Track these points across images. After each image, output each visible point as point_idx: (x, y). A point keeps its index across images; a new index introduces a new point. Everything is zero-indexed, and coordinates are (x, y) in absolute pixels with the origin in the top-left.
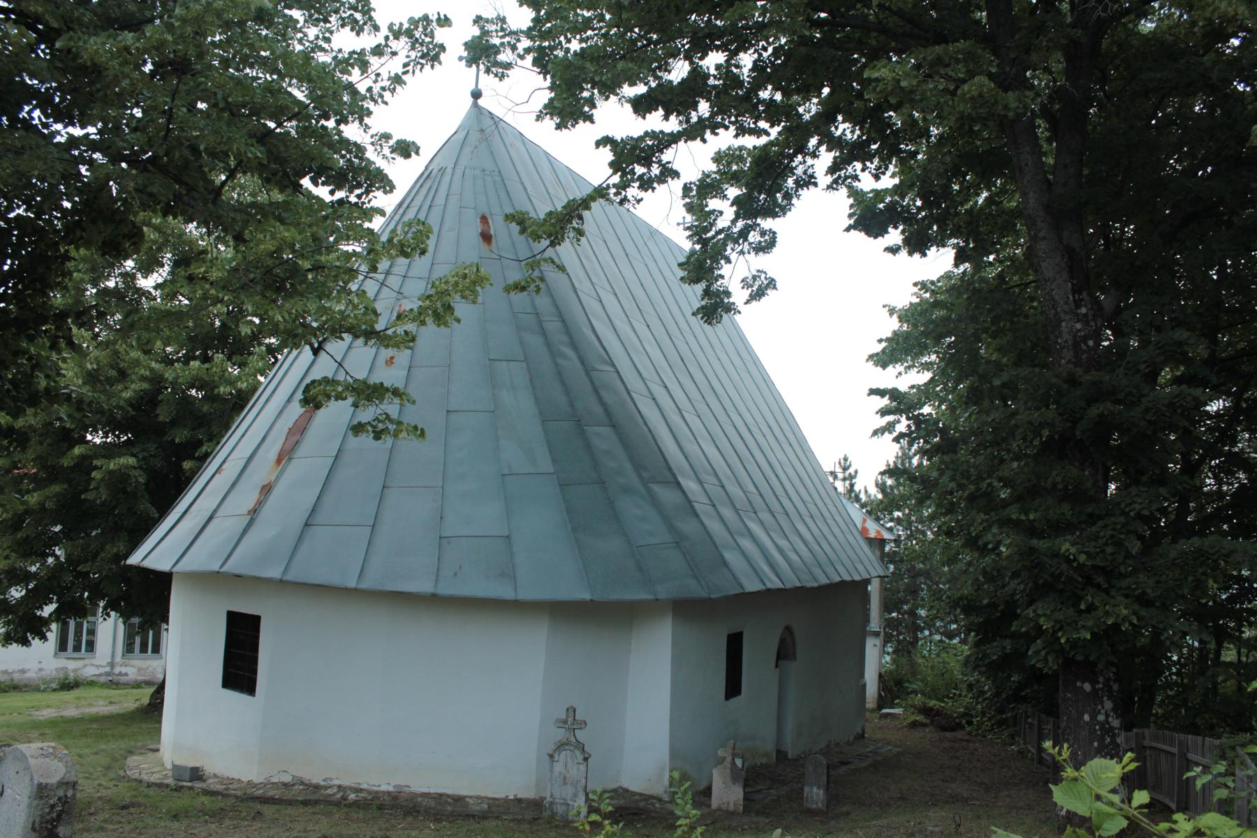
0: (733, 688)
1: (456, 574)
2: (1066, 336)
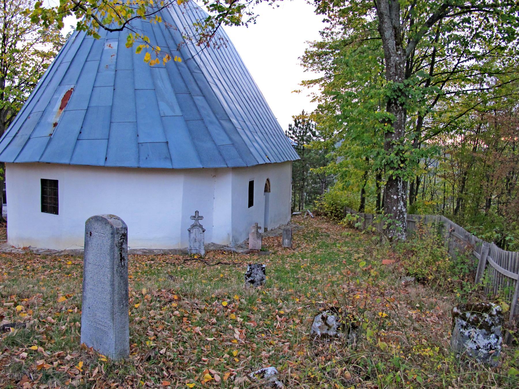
0: (251, 204)
1: (147, 158)
2: (392, 62)
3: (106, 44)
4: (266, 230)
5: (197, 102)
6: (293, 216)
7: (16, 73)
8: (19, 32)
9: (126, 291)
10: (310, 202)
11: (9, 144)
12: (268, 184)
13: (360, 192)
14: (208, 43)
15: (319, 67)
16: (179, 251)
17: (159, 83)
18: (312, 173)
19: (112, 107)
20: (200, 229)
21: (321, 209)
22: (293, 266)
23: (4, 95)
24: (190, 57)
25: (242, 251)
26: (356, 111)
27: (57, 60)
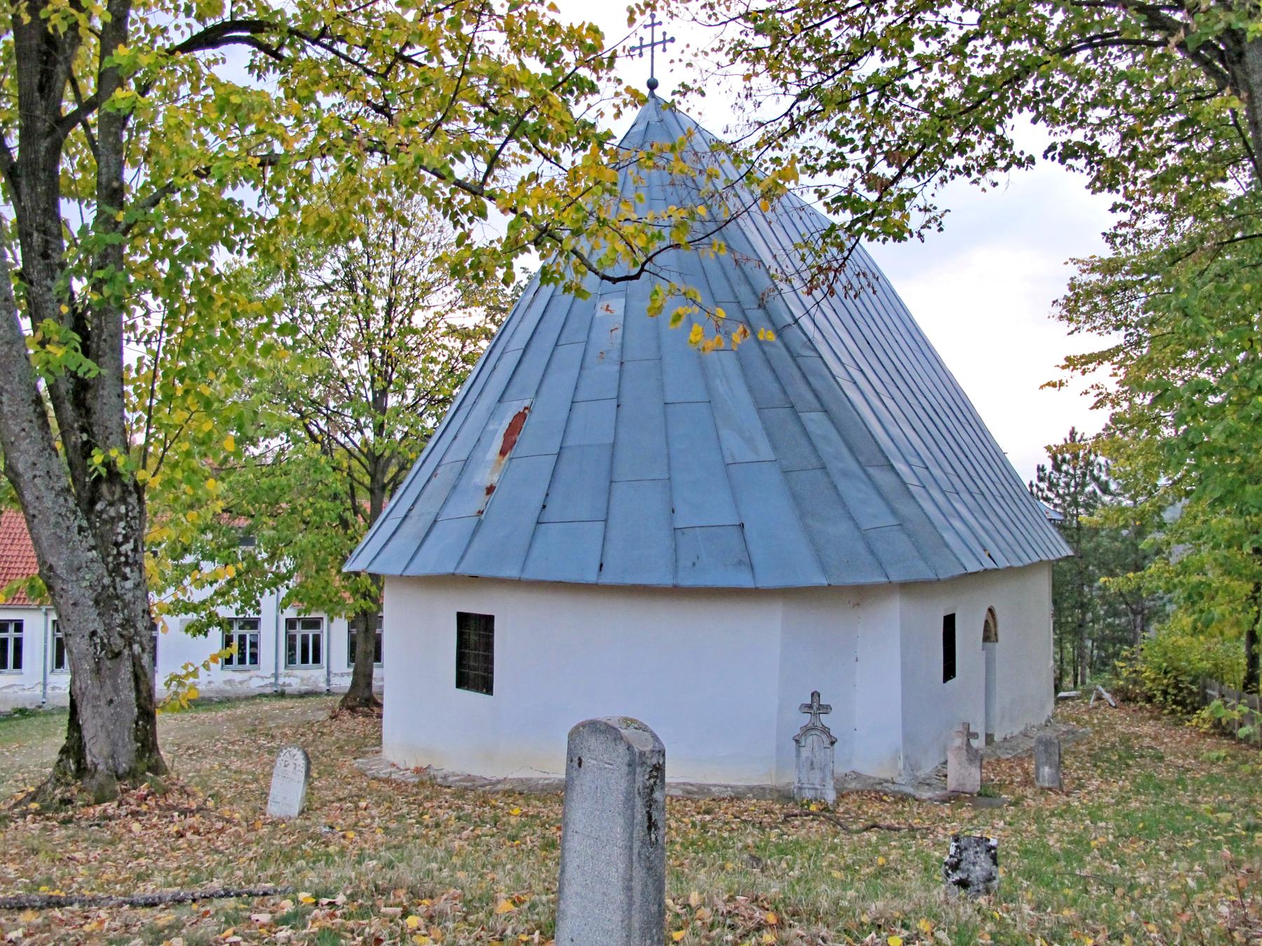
1: (694, 564)
3: (598, 307)
4: (989, 738)
5: (811, 427)
6: (1058, 700)
7: (409, 377)
8: (418, 292)
9: (660, 905)
10: (1105, 664)
11: (394, 533)
12: (992, 624)
13: (1244, 638)
14: (830, 287)
15: (1108, 321)
16: (771, 790)
17: (720, 386)
18: (1104, 588)
19: (614, 445)
20: (824, 737)
21: (1135, 682)
22: (1070, 842)
23: (386, 426)
24: (790, 320)
25: (929, 794)
26: (1219, 428)
27: (494, 346)
